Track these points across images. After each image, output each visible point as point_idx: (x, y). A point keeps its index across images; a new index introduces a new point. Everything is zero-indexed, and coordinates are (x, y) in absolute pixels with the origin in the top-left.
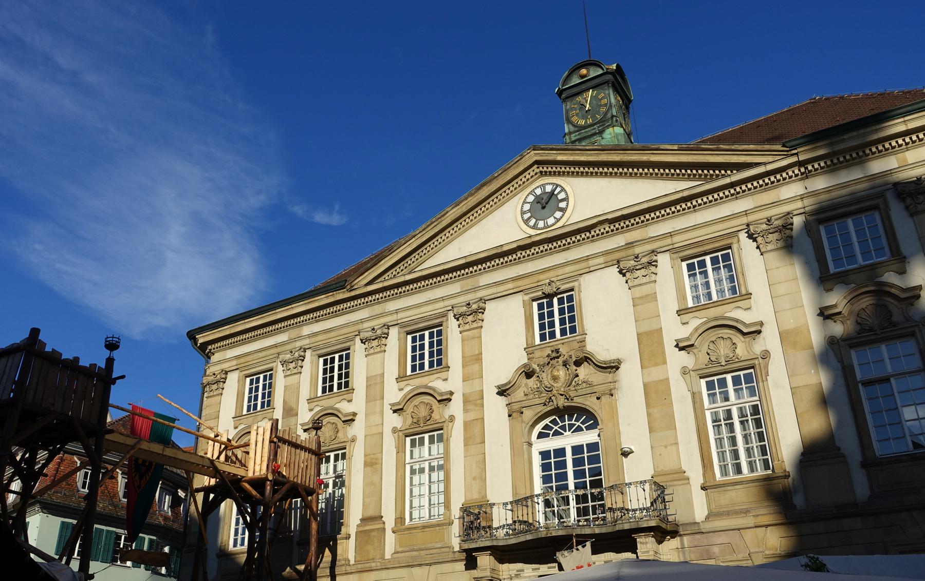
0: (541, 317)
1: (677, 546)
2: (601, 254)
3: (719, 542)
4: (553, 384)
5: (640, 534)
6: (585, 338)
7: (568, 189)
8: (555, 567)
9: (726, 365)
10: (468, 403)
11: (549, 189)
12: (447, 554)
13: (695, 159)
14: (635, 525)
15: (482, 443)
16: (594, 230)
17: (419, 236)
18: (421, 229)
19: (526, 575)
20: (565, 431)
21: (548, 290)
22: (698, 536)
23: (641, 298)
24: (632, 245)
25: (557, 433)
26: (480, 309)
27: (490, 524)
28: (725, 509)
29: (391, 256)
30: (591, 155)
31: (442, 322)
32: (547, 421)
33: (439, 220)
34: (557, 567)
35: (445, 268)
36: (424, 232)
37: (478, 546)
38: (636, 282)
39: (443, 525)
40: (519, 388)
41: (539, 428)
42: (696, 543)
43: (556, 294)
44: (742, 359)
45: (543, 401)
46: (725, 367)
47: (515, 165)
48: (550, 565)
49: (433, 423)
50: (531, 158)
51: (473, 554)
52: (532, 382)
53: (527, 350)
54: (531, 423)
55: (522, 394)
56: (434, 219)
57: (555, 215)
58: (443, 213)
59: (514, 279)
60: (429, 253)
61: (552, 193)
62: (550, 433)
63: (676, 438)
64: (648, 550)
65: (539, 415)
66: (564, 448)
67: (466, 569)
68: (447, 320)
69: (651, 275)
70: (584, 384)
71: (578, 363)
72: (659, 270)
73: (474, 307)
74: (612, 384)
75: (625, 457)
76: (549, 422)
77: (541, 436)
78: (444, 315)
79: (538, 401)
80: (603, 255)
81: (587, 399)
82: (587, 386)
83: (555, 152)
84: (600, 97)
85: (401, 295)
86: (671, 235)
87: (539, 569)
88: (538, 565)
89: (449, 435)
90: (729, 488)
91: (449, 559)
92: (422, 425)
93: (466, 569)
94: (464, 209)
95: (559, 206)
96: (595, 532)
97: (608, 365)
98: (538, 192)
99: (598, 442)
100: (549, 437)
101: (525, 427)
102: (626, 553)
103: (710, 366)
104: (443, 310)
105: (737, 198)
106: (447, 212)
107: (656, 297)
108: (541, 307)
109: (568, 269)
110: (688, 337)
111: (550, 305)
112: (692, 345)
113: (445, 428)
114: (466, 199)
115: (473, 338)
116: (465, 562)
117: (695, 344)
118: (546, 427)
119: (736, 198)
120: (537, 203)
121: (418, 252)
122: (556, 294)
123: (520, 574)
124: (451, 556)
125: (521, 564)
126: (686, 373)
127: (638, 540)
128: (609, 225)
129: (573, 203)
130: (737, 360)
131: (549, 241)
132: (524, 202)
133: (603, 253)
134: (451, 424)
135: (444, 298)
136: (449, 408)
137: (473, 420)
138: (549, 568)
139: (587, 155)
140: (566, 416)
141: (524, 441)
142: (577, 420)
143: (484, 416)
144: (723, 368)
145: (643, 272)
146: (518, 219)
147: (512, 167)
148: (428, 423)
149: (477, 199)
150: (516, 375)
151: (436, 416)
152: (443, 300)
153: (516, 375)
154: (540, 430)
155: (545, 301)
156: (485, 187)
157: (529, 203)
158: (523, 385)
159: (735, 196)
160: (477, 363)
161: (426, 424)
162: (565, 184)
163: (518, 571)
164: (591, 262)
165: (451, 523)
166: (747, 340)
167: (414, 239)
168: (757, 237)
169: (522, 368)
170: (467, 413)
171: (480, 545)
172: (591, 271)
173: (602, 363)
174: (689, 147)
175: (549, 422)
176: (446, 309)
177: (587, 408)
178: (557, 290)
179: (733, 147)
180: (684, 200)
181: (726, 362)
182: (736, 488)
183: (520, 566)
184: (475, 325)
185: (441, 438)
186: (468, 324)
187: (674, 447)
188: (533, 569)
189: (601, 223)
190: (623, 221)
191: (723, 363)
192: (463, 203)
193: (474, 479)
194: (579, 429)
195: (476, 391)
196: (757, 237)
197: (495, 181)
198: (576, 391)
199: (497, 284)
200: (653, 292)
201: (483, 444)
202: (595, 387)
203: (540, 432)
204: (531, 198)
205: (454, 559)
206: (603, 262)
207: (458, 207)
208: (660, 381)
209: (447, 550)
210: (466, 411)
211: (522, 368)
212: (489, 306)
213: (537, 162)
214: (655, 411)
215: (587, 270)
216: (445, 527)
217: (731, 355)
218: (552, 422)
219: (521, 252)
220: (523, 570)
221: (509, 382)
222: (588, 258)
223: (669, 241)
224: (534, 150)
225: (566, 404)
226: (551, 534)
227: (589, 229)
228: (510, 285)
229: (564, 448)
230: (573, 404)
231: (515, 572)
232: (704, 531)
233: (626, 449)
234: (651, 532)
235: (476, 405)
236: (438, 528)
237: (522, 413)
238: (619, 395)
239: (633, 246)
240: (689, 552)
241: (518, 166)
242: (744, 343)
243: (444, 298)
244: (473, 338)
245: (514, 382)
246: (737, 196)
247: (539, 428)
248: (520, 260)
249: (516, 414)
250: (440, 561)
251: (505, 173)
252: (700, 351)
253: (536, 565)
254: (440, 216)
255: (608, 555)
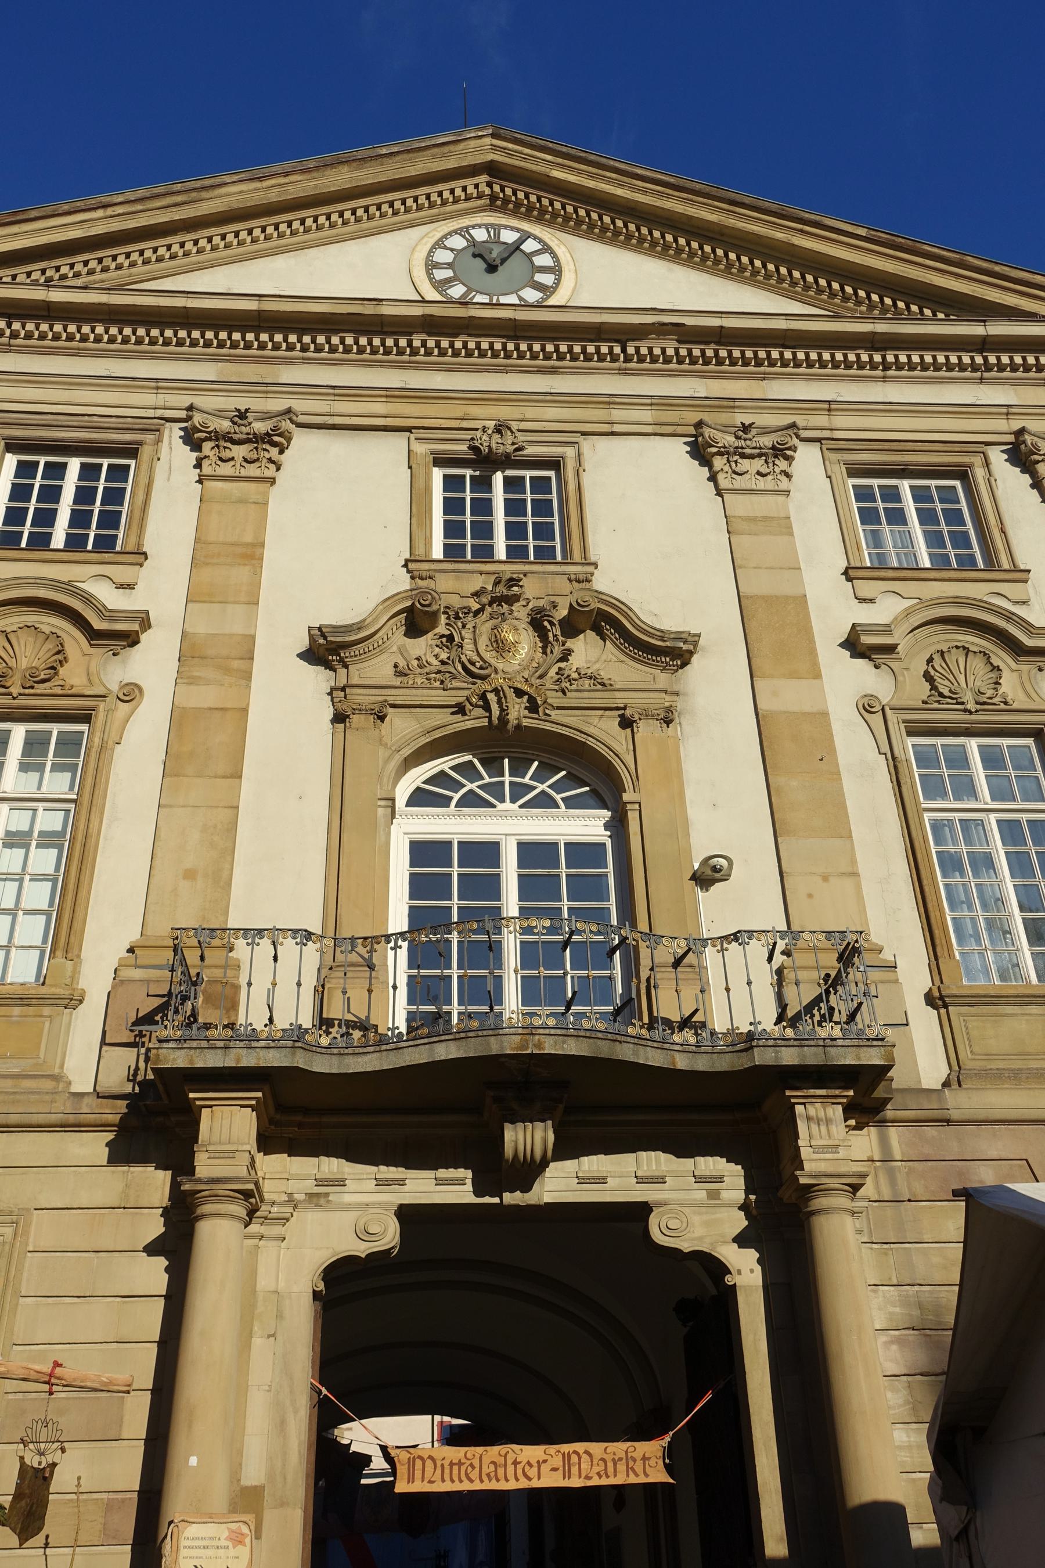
0: (452, 506)
1: (869, 1154)
2: (649, 401)
3: (994, 1154)
4: (493, 661)
5: (812, 1092)
6: (592, 574)
7: (561, 251)
8: (461, 1182)
9: (977, 711)
10: (196, 660)
11: (509, 237)
12: (47, 1098)
13: (903, 271)
14: (816, 1054)
15: (232, 777)
16: (637, 344)
17: (119, 210)
18: (131, 195)
19: (348, 1198)
20: (502, 801)
21: (486, 442)
22: (931, 1131)
23: (753, 520)
24: (731, 404)
25: (471, 801)
26: (279, 435)
27: (232, 1021)
28: (1001, 1065)
29: (15, 229)
30: (644, 191)
31: (140, 443)
32: (444, 764)
33: (194, 195)
34: (469, 1182)
35: (188, 306)
36: (139, 207)
37: (230, 1063)
38: (740, 482)
39: (42, 1001)
40: (382, 652)
41: (417, 776)
42: (928, 1151)
43: (506, 461)
44: (1015, 706)
45: (453, 701)
46: (973, 717)
47: (436, 150)
48: (442, 1173)
49: (58, 691)
50: (479, 150)
51: (192, 1095)
52: (422, 647)
53: (411, 566)
54: (407, 752)
55: (390, 671)
56: (178, 187)
57: (521, 293)
58: (208, 182)
59: (391, 394)
60: (133, 270)
61: (516, 247)
62: (483, 778)
63: (853, 861)
64: (837, 1143)
65: (438, 734)
66: (497, 844)
67: (115, 1159)
68: (159, 441)
69: (779, 477)
70: (587, 682)
71: (571, 627)
72: (796, 469)
73: (261, 427)
74: (668, 698)
75: (702, 889)
76: (451, 768)
77: (419, 798)
78: (153, 427)
79: (438, 696)
80: (651, 405)
81: (589, 720)
82: (593, 687)
83: (549, 157)
84: (449, 273)
85: (13, 342)
86: (830, 407)
87: (401, 1182)
88: (402, 1169)
89: (114, 736)
90: (1009, 1009)
91: (53, 1118)
92: (15, 690)
93: (115, 1159)
94: (274, 196)
95: (536, 278)
96: (674, 1063)
97: (668, 644)
98: (480, 235)
99: (604, 844)
100: (448, 806)
101: (387, 761)
102: (710, 1159)
103: (936, 705)
104: (150, 413)
105: (981, 380)
106: (223, 185)
107: (790, 527)
108: (452, 483)
109: (553, 412)
110: (888, 625)
111: (483, 484)
112: (890, 649)
113: (99, 719)
114: (286, 174)
115: (242, 501)
116: (111, 1136)
117: (899, 648)
118: (441, 778)
119: (981, 378)
120: (475, 256)
121: (100, 254)
122: (506, 461)
123: (327, 1194)
124: (61, 1109)
125: (334, 1161)
126: (873, 710)
127: (799, 1109)
128: (677, 345)
129: (573, 285)
130: (1002, 706)
131: (512, 334)
132: (437, 243)
133: (654, 401)
134: (124, 708)
135: (161, 384)
136: (124, 662)
137: (210, 709)
138: (440, 1182)
139: (633, 189)
140: (506, 761)
141: (380, 793)
142: (537, 777)
143: (248, 704)
144: (967, 717)
145: (758, 464)
146: (415, 274)
147: (429, 152)
148: (40, 689)
149: (316, 187)
150: (381, 614)
151: (73, 675)
152: (157, 388)
153: (381, 614)
154: (419, 783)
155: (468, 473)
156: (345, 168)
157: (452, 250)
158: (395, 648)
159: (978, 374)
160: (245, 565)
161: (31, 691)
162: (553, 241)
163: (320, 1182)
164: (617, 414)
165: (74, 1001)
166: (1025, 668)
167: (100, 213)
168: (1038, 462)
169: (404, 599)
170: (192, 687)
171: (238, 1061)
172: (613, 434)
173: (652, 635)
174: (894, 241)
175: (451, 768)
176: (159, 413)
177: (591, 742)
178: (516, 450)
179: (997, 268)
180: (869, 345)
181: (977, 703)
182: (1027, 1012)
183: (331, 1166)
184: (252, 470)
185: (69, 745)
186: (232, 463)
187: (848, 883)
188: (380, 1182)
189: (662, 330)
190: (713, 346)
191: (971, 706)
192: (273, 182)
193: (190, 875)
194: (544, 802)
195: (231, 635)
196: (1038, 462)
197: (373, 163)
198: (560, 694)
199: (337, 391)
200: (782, 515)
201: (237, 780)
202: (618, 695)
203: (418, 789)
204: (458, 242)
205: (71, 1119)
206: (650, 420)
207: (257, 185)
208: (804, 714)
209: (48, 1085)
210: (184, 676)
211: (404, 599)
212: (302, 442)
213: (492, 169)
214: (794, 783)
215: (605, 428)
216: (46, 1011)
217: (990, 693)
218: (463, 769)
219: (424, 337)
220: (341, 1183)
221: (359, 626)
222: (611, 401)
223: (822, 420)
224: (493, 136)
225: (526, 722)
226: (539, 1045)
227: (623, 337)
228: (379, 407)
229: (497, 844)
230: (547, 726)
231: (310, 1186)
232: (955, 1115)
233: (721, 860)
234: (846, 1088)
235: (227, 671)
236: (16, 1011)
237: (382, 718)
238: (685, 727)
239: (734, 407)
240: (908, 1174)
241: (444, 156)
242: (1015, 674)
243: (161, 384)
244: (242, 501)
245: (372, 630)
246: (986, 375)
247: (417, 776)
248: (413, 358)
249: (363, 717)
250: (13, 1119)
251: (405, 156)
252: (907, 669)
253: (392, 1169)
254: (198, 184)
255: (649, 1159)
